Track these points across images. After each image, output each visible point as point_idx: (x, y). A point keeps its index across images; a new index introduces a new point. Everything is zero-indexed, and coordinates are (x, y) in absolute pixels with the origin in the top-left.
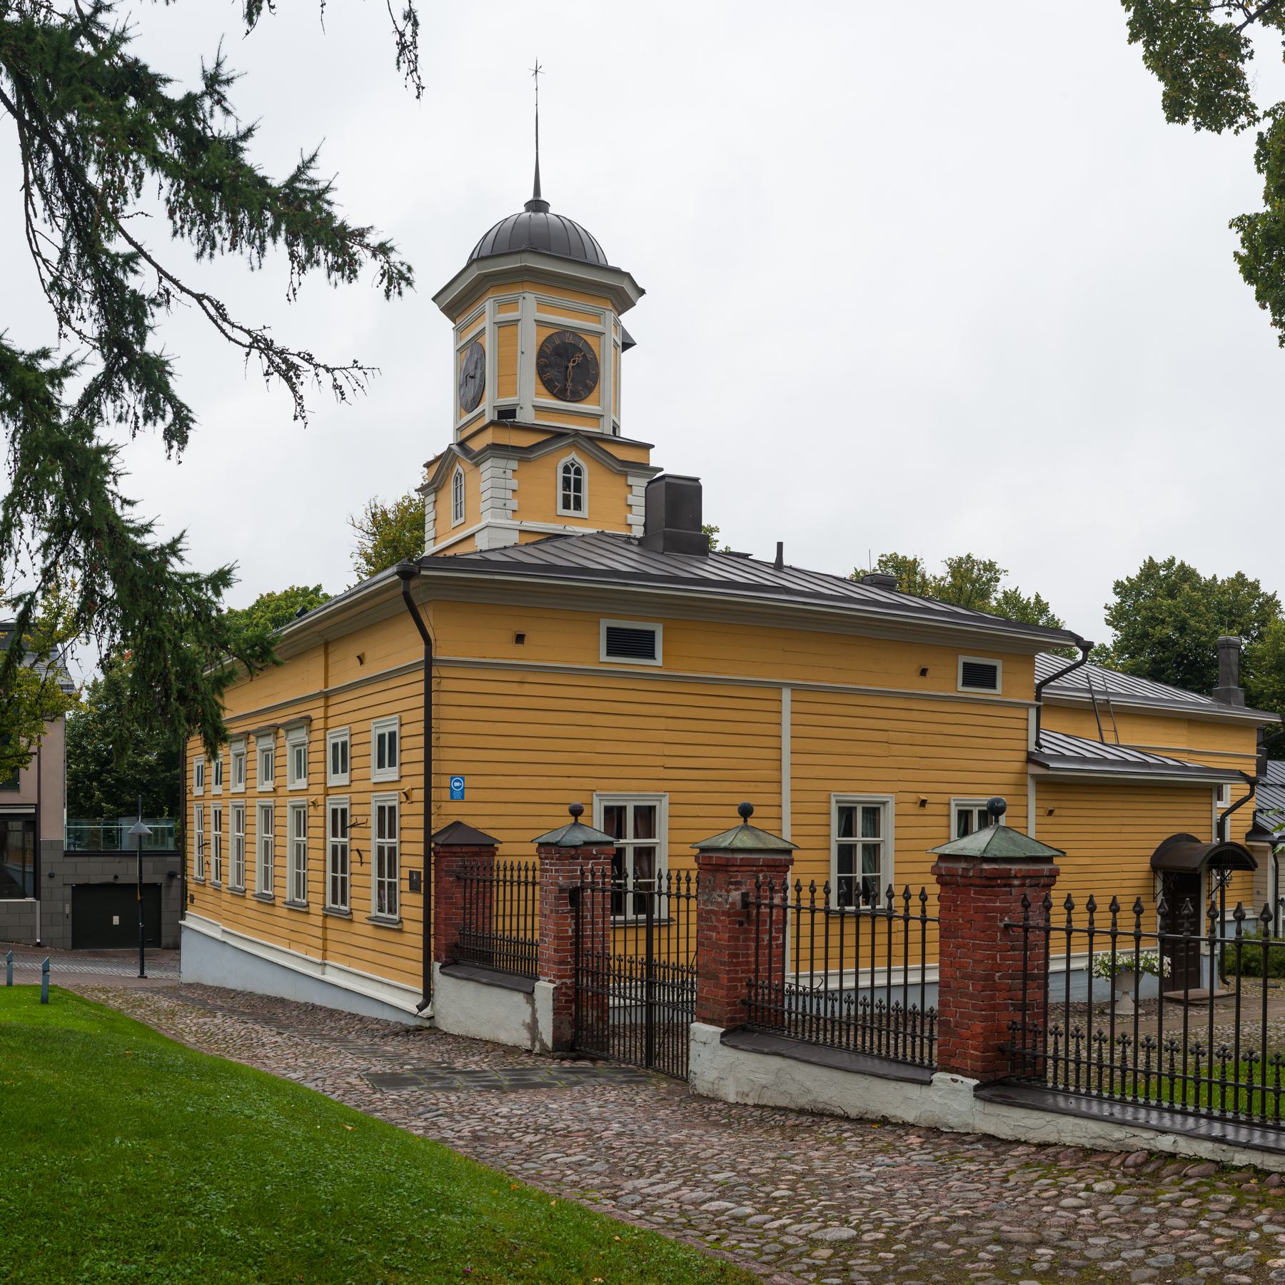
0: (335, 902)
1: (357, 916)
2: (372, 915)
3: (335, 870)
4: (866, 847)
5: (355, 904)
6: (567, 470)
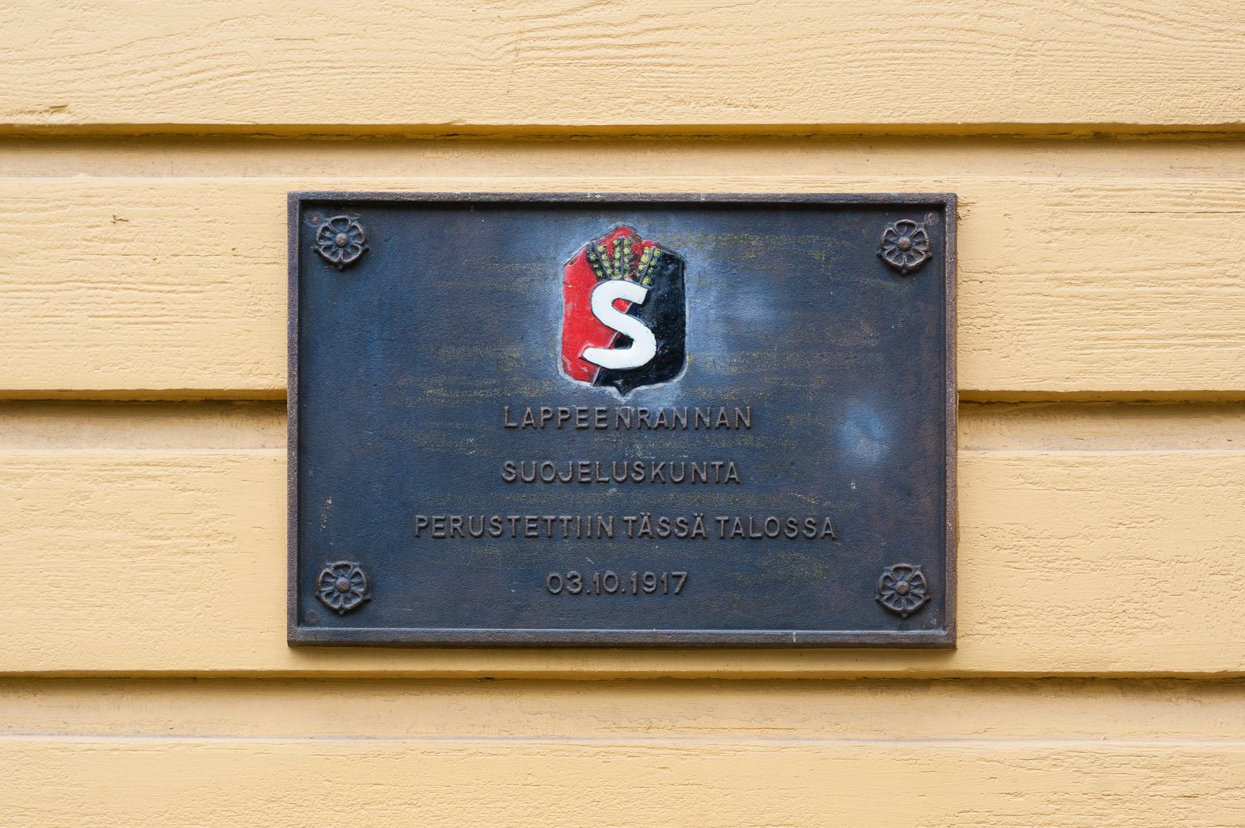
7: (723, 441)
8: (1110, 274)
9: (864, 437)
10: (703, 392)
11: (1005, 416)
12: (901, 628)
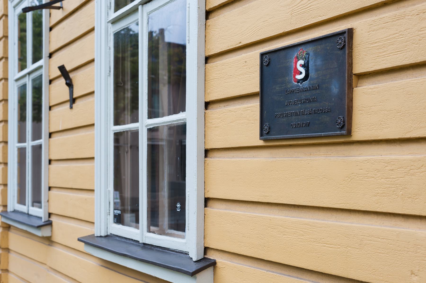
0: (22, 200)
1: (62, 230)
2: (99, 230)
3: (22, 138)
5: (56, 202)
7: (314, 92)
8: (380, 40)
9: (335, 89)
10: (312, 82)
11: (367, 78)
12: (340, 131)
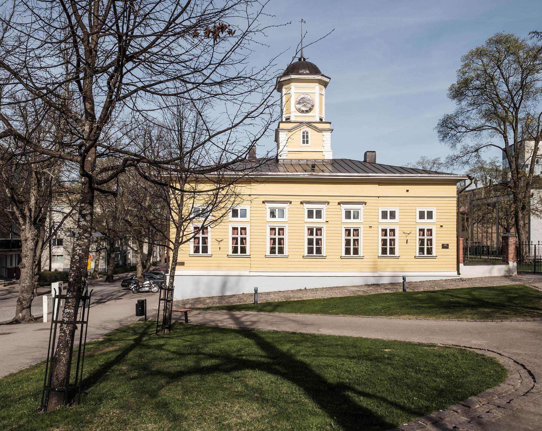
4: (354, 240)
6: (304, 133)
